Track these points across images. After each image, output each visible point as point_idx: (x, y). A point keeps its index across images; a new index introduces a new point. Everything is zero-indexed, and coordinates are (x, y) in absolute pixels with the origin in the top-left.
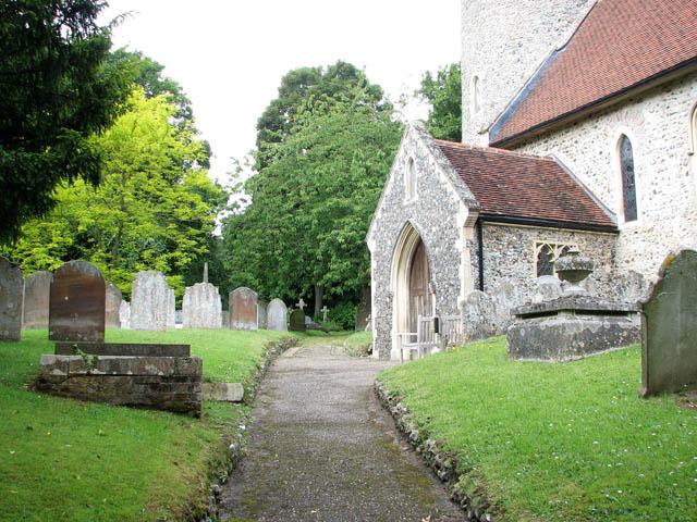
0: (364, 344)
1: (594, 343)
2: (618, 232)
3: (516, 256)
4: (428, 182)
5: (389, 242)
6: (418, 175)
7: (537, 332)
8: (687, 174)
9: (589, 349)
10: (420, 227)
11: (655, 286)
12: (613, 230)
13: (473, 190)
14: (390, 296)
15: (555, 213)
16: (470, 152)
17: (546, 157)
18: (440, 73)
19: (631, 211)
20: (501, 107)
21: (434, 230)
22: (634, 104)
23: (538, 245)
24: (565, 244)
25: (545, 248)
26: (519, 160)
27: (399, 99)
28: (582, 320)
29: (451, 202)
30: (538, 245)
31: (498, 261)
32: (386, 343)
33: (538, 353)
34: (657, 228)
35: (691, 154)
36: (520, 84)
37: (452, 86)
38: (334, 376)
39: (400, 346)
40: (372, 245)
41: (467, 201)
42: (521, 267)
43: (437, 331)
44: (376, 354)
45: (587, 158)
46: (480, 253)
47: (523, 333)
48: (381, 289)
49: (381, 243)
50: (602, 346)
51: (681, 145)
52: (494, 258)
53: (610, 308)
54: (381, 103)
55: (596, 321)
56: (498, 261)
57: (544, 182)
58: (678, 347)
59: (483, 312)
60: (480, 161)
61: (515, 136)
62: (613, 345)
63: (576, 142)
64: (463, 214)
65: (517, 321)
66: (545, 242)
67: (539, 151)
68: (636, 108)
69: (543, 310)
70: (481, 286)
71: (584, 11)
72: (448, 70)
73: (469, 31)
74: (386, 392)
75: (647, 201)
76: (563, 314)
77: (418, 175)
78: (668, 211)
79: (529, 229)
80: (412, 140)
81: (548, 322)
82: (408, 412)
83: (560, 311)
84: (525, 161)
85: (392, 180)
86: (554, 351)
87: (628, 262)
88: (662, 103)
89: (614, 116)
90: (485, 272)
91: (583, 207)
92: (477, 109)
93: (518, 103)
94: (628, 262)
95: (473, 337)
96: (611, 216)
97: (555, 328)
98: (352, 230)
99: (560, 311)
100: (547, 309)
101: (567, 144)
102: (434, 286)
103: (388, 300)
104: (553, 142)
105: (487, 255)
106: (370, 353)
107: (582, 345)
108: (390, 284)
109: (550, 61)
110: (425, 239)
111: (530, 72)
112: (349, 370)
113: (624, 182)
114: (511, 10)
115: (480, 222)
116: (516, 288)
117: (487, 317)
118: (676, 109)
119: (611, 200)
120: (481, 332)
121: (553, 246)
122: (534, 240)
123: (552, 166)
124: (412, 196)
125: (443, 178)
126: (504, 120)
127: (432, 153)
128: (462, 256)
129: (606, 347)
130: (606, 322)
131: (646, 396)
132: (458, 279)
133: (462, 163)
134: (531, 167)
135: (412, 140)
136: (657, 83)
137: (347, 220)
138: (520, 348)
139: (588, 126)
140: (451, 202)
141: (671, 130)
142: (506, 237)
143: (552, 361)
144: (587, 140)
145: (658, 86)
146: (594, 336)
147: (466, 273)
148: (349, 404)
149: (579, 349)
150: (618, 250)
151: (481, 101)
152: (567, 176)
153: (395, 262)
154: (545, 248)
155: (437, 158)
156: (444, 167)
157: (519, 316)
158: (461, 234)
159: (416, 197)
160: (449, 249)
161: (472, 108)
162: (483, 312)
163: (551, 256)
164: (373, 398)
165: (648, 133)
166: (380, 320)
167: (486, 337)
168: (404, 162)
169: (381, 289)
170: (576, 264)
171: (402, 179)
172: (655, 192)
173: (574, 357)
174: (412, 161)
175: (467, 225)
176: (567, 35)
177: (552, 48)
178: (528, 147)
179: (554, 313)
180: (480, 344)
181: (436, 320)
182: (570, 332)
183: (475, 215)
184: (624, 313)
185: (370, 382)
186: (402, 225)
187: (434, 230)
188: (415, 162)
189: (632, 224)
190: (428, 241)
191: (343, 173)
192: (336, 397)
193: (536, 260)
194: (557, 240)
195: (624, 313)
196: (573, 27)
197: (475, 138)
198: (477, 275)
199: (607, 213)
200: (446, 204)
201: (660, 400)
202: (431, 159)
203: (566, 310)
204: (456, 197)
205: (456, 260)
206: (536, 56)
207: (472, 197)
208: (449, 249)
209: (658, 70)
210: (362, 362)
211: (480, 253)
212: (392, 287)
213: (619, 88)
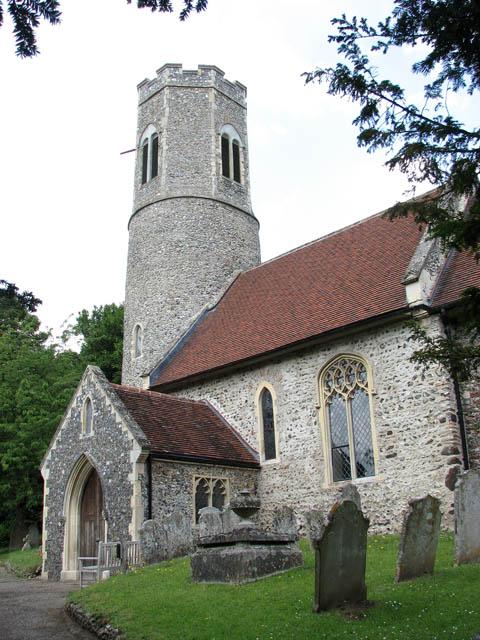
0: (32, 564)
1: (265, 567)
2: (260, 468)
3: (181, 486)
4: (105, 420)
5: (63, 472)
6: (95, 414)
7: (218, 560)
8: (315, 423)
9: (260, 573)
10: (95, 460)
11: (327, 528)
12: (256, 467)
13: (145, 430)
14: (63, 521)
15: (210, 452)
16: (138, 396)
17: (200, 401)
18: (94, 312)
19: (270, 452)
20: (160, 355)
21: (108, 463)
22: (275, 363)
23: (197, 479)
24: (218, 478)
25: (203, 481)
26: (179, 403)
27: (61, 334)
28: (254, 549)
29: (125, 440)
30: (197, 479)
31: (164, 492)
32: (56, 565)
33: (218, 577)
34: (292, 465)
35: (318, 408)
36: (178, 336)
37: (106, 325)
38: (20, 600)
39: (70, 570)
40: (45, 473)
41: (140, 441)
42: (182, 498)
43: (119, 556)
44: (44, 575)
45: (235, 406)
46: (149, 486)
47: (205, 560)
48: (53, 514)
49: (55, 472)
50: (270, 570)
51: (310, 400)
52: (161, 490)
53: (275, 539)
54: (37, 333)
55: (265, 549)
56: (164, 492)
57: (200, 424)
58: (341, 572)
59: (157, 539)
60: (146, 403)
61: (174, 382)
62: (278, 569)
63: (226, 391)
64: (136, 453)
65: (198, 550)
66: (202, 476)
67: (195, 396)
68: (275, 368)
69: (223, 541)
70: (149, 515)
71: (230, 280)
72: (103, 310)
73: (135, 286)
74: (88, 615)
75: (283, 443)
76: (240, 545)
77: (95, 414)
78: (300, 452)
79: (189, 465)
80: (90, 383)
81: (226, 551)
82: (120, 633)
83: (238, 542)
84: (184, 405)
85: (69, 416)
86: (233, 576)
87: (268, 493)
88: (296, 366)
89: (258, 372)
90: (153, 502)
91: (232, 446)
92: (138, 354)
93: (174, 352)
94: (268, 493)
95: (150, 561)
96: (254, 454)
97: (233, 556)
98: (15, 455)
99: (238, 542)
100: (227, 541)
101: (218, 392)
102: (106, 513)
103: (60, 524)
104: (205, 389)
105: (155, 487)
106: (39, 573)
107: (256, 569)
108: (64, 514)
109: (202, 318)
110: (99, 470)
111: (185, 327)
112: (30, 593)
113: (265, 426)
114: (171, 273)
115: (149, 460)
116: (184, 519)
117: (161, 543)
118: (307, 371)
119: (256, 443)
120: (155, 557)
121: (209, 479)
122: (194, 475)
123: (205, 410)
124: (88, 431)
125: (118, 419)
126: (163, 367)
127: (109, 396)
128: (134, 489)
129: (274, 571)
130: (271, 550)
131: (318, 611)
132: (130, 509)
133: (130, 401)
134: (189, 410)
135: (90, 383)
136: (293, 349)
137: (10, 444)
138: (202, 572)
139: (236, 379)
140: (125, 440)
141: (303, 388)
142: (172, 472)
143: (231, 583)
144: (235, 390)
145: (294, 352)
146: (264, 561)
147: (136, 501)
148: (51, 628)
149: (253, 573)
150: (260, 483)
151: (141, 347)
152: (218, 419)
153: (70, 486)
154: (203, 481)
155: (113, 401)
156: (119, 409)
157: (200, 546)
158: (134, 469)
159: (92, 433)
160: (122, 480)
161: (133, 352)
162: (157, 539)
163: (223, 489)
164: (70, 622)
165: (285, 388)
166: (51, 544)
167: (160, 561)
168: (81, 401)
169: (53, 514)
170: (248, 503)
171: (79, 416)
172: (290, 436)
173: (250, 580)
174: (88, 401)
175: (139, 461)
176: (216, 299)
177: (204, 307)
178: (184, 392)
179: (232, 544)
180: (158, 568)
181: (118, 547)
182: (247, 560)
183: (147, 453)
184: (285, 543)
185: (62, 602)
186: (77, 457)
187: (108, 463)
188: (92, 402)
189: (271, 462)
190: (103, 473)
191: (8, 400)
192: (35, 621)
193: (194, 491)
194: (212, 475)
195: (285, 543)
196: (222, 292)
197: (136, 377)
198: (147, 504)
199: (251, 452)
200: (121, 442)
201: (329, 614)
202: (108, 402)
203: (242, 542)
204: (130, 436)
205: (129, 491)
206: (191, 315)
207: (144, 437)
208: (122, 480)
209: (294, 340)
210: (33, 583)
211: (149, 486)
212: (65, 513)
213: (263, 351)
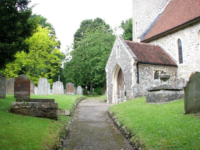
0: (105, 99)
1: (171, 98)
2: (177, 67)
3: (148, 74)
4: (123, 52)
5: (112, 70)
6: (120, 50)
7: (154, 95)
8: (197, 50)
9: (169, 100)
10: (121, 65)
11: (188, 82)
12: (176, 66)
13: (136, 55)
14: (112, 85)
15: (159, 61)
16: (135, 44)
17: (157, 45)
18: (126, 21)
19: (181, 61)
20: (144, 31)
21: (124, 66)
22: (182, 30)
23: (154, 70)
24: (162, 70)
25: (157, 71)
26: (149, 46)
27: (114, 28)
28: (167, 92)
29: (129, 58)
30: (154, 70)
31: (143, 75)
32: (111, 99)
33: (154, 101)
34: (189, 65)
35: (198, 44)
36: (149, 24)
37: (130, 25)
38: (96, 108)
39: (115, 99)
40: (107, 70)
41: (134, 58)
42: (150, 77)
43: (125, 95)
44: (108, 102)
45: (168, 46)
46: (138, 73)
47: (150, 96)
48: (109, 83)
49: (109, 70)
50: (173, 99)
51: (195, 42)
52: (142, 74)
53: (175, 89)
54: (109, 30)
55: (171, 92)
56: (143, 75)
57: (156, 52)
58: (195, 100)
59: (139, 90)
60: (138, 46)
61: (148, 39)
62: (176, 99)
63: (165, 41)
64: (133, 62)
65: (148, 92)
66: (156, 70)
67: (155, 43)
68: (183, 31)
69: (156, 89)
70: (138, 82)
71: (168, 3)
72: (129, 20)
73: (135, 9)
74: (111, 113)
75: (186, 58)
76: (161, 90)
77: (120, 50)
78: (192, 61)
79: (152, 66)
80: (118, 40)
81: (157, 92)
82: (117, 118)
83: (161, 89)
84: (151, 46)
85: (112, 52)
86: (159, 101)
87: (180, 75)
88: (190, 30)
89: (176, 33)
90: (139, 78)
91: (167, 59)
92: (137, 31)
93: (149, 30)
94: (180, 75)
95: (136, 97)
96: (175, 62)
97: (159, 94)
98: (101, 66)
99: (161, 89)
100: (157, 89)
101: (163, 41)
102: (124, 82)
103: (111, 86)
104: (159, 41)
105: (140, 73)
106: (106, 101)
107: (167, 99)
108: (112, 82)
109: (158, 17)
110: (122, 69)
111: (152, 21)
112: (100, 106)
113: (179, 52)
114: (147, 3)
115: (138, 64)
116: (148, 83)
117: (140, 91)
118: (194, 31)
119: (175, 58)
120: (138, 95)
121: (159, 71)
122: (153, 69)
123: (158, 48)
124: (118, 56)
125: (127, 51)
126: (145, 34)
127: (124, 44)
128: (133, 74)
129: (174, 100)
130: (174, 93)
131: (185, 114)
132: (131, 80)
133: (133, 47)
134: (152, 48)
135: (118, 40)
136: (188, 24)
137: (100, 63)
138: (149, 100)
139: (169, 36)
140: (129, 58)
141: (193, 37)
142: (145, 68)
143: (158, 104)
144: (168, 40)
145: (189, 25)
146: (171, 96)
147: (134, 78)
148: (100, 116)
149: (166, 100)
150: (177, 72)
151: (138, 29)
152: (163, 50)
153: (113, 75)
154: (157, 71)
155: (125, 45)
156: (127, 48)
157: (149, 91)
158: (132, 67)
159: (119, 57)
160: (129, 71)
161: (135, 31)
162: (139, 90)
163: (158, 74)
164: (107, 114)
165: (186, 38)
166: (109, 92)
167: (140, 97)
168: (116, 47)
169: (109, 83)
170: (165, 76)
171: (115, 51)
172: (188, 55)
173: (165, 103)
174: (118, 46)
175: (134, 65)
176: (163, 10)
177: (158, 14)
178: (152, 42)
179: (159, 90)
180: (138, 99)
181: (125, 92)
182: (164, 96)
183: (136, 62)
184: (179, 90)
185: (106, 110)
186: (115, 65)
187: (124, 66)
188: (119, 46)
189: (181, 64)
190: (123, 69)
191: (98, 50)
192: (96, 114)
193: (154, 75)
194: (160, 69)
195: (179, 90)
196: (165, 8)
197: (136, 40)
198: (137, 79)
199: (174, 61)
200: (128, 59)
201: (189, 115)
202: (124, 46)
203: (162, 89)
204: (131, 57)
205: (131, 75)
206: (154, 16)
207: (135, 57)
208: (129, 71)
209: (189, 20)
210: (104, 104)
211: (138, 73)
212: (112, 83)
213: (178, 25)
